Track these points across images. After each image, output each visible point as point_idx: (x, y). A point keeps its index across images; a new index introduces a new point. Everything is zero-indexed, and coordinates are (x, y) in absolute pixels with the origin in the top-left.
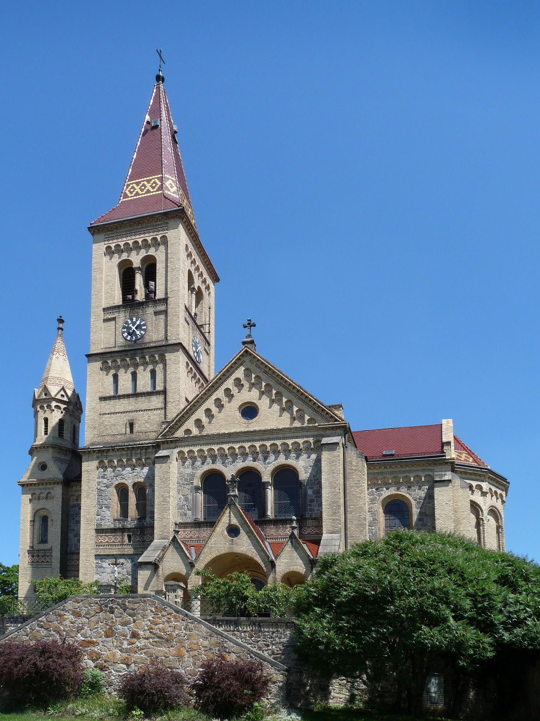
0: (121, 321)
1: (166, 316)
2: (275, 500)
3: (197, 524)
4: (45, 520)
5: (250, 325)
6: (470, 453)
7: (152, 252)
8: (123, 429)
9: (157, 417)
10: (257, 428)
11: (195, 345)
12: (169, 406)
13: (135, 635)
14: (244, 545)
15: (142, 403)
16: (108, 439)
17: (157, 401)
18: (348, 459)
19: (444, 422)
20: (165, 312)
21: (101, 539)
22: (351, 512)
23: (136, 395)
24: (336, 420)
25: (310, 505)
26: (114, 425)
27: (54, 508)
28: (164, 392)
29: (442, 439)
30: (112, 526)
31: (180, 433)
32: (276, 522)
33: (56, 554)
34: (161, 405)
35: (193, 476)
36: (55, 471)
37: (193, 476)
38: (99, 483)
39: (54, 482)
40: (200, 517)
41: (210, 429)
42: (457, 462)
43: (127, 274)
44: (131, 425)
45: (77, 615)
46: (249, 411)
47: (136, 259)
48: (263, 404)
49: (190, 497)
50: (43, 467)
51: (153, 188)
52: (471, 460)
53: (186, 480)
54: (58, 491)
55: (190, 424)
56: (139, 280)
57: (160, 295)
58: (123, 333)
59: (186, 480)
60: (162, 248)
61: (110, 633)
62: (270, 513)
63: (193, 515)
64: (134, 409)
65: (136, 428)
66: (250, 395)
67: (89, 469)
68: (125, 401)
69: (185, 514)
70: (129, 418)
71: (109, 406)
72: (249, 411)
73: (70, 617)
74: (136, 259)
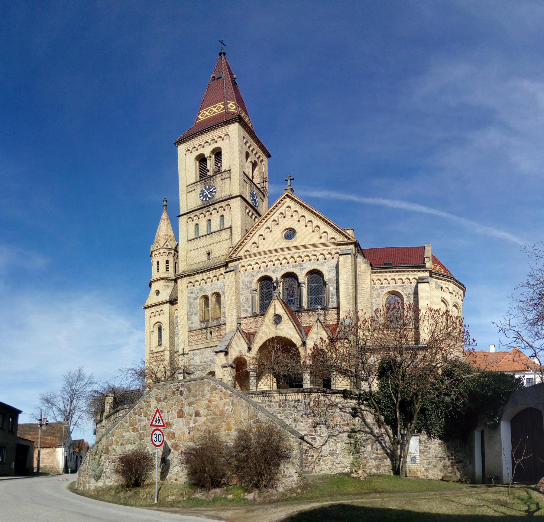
0: (199, 191)
1: (231, 231)
2: (308, 295)
3: (255, 316)
4: (160, 329)
6: (442, 266)
7: (219, 144)
8: (205, 258)
10: (295, 245)
11: (253, 196)
12: (234, 236)
14: (286, 329)
15: (216, 238)
17: (225, 235)
18: (358, 265)
19: (426, 245)
20: (229, 177)
21: (192, 338)
22: (360, 303)
24: (349, 239)
25: (332, 298)
26: (198, 257)
28: (230, 227)
30: (200, 327)
31: (241, 253)
32: (308, 310)
34: (228, 237)
35: (251, 282)
37: (251, 282)
38: (189, 298)
40: (258, 313)
42: (433, 271)
43: (202, 160)
44: (209, 254)
45: (159, 400)
46: (290, 234)
47: (207, 151)
48: (299, 228)
49: (250, 298)
51: (218, 110)
52: (443, 270)
53: (246, 285)
58: (200, 197)
59: (246, 285)
60: (226, 140)
61: (181, 414)
62: (305, 305)
63: (252, 310)
64: (210, 243)
65: (212, 255)
66: (291, 223)
68: (203, 240)
69: (247, 311)
70: (207, 250)
71: (192, 245)
74: (207, 151)
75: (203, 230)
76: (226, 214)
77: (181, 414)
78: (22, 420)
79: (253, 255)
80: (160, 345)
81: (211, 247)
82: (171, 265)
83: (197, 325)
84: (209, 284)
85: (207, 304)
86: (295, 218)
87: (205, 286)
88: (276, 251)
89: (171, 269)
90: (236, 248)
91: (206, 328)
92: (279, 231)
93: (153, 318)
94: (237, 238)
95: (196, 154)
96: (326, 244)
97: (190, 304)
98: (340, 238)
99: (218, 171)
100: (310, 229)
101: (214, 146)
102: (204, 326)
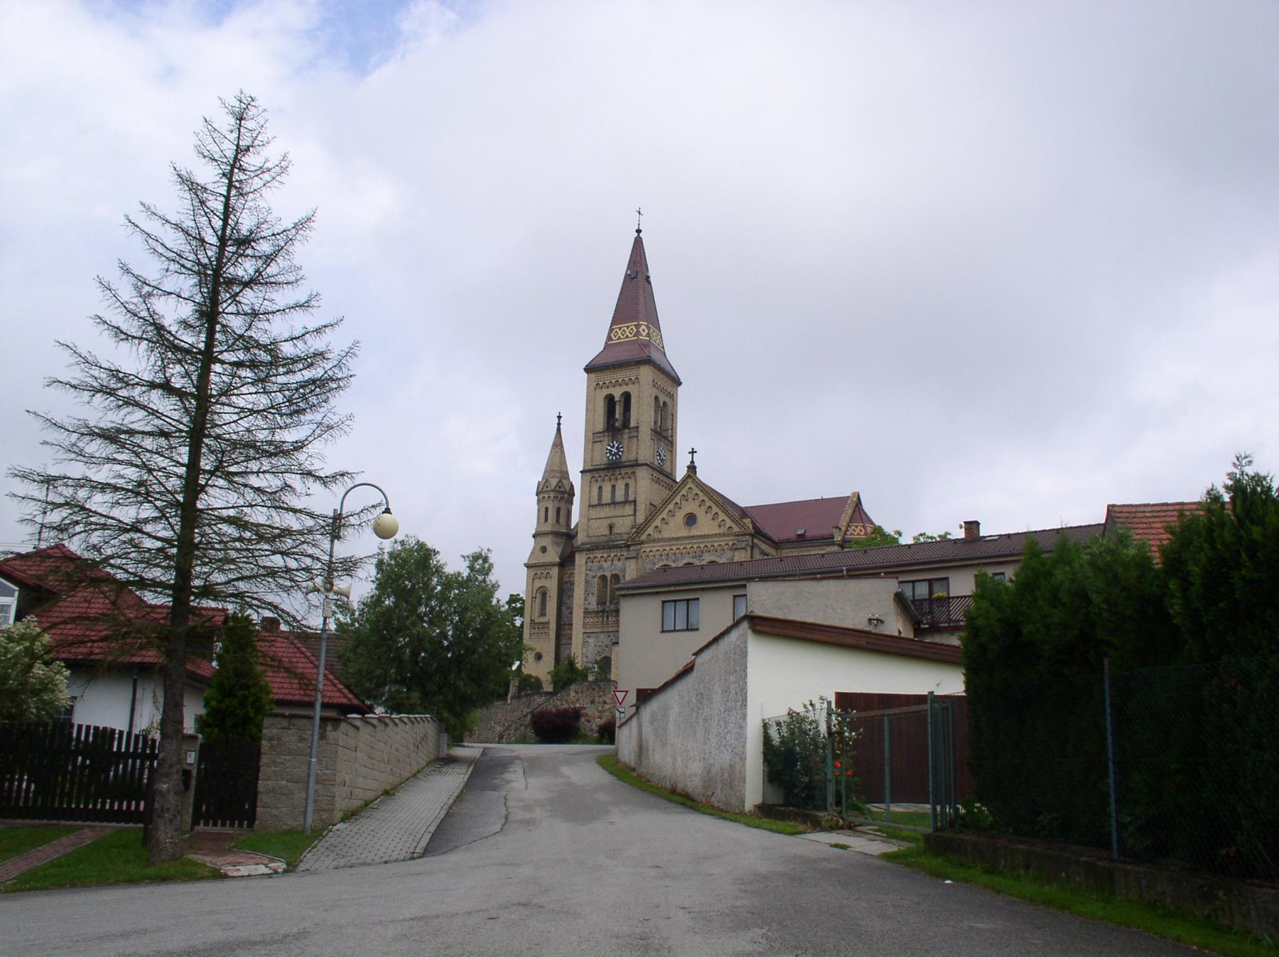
4: (544, 595)
5: (693, 452)
9: (628, 522)
13: (605, 702)
15: (619, 511)
16: (594, 539)
17: (629, 509)
23: (613, 503)
27: (552, 585)
28: (635, 501)
29: (764, 579)
31: (643, 537)
33: (553, 626)
36: (553, 556)
39: (552, 565)
41: (666, 534)
45: (577, 692)
46: (691, 519)
47: (617, 393)
48: (700, 514)
50: (544, 549)
54: (555, 572)
55: (650, 530)
56: (619, 410)
57: (633, 424)
61: (593, 702)
65: (615, 530)
66: (690, 507)
67: (580, 559)
68: (606, 509)
71: (594, 513)
72: (691, 519)
73: (572, 694)
74: (617, 393)
75: (606, 497)
76: (631, 482)
77: (593, 702)
78: (203, 711)
79: (654, 541)
80: (543, 614)
81: (614, 520)
82: (563, 513)
83: (593, 606)
84: (609, 563)
85: (605, 586)
86: (697, 502)
87: (606, 565)
88: (677, 539)
89: (563, 520)
90: (640, 529)
91: (603, 611)
92: (680, 516)
93: (537, 581)
94: (641, 518)
95: (606, 392)
96: (724, 535)
97: (587, 582)
98: (736, 529)
99: (626, 424)
100: (710, 516)
101: (625, 389)
102: (601, 608)
